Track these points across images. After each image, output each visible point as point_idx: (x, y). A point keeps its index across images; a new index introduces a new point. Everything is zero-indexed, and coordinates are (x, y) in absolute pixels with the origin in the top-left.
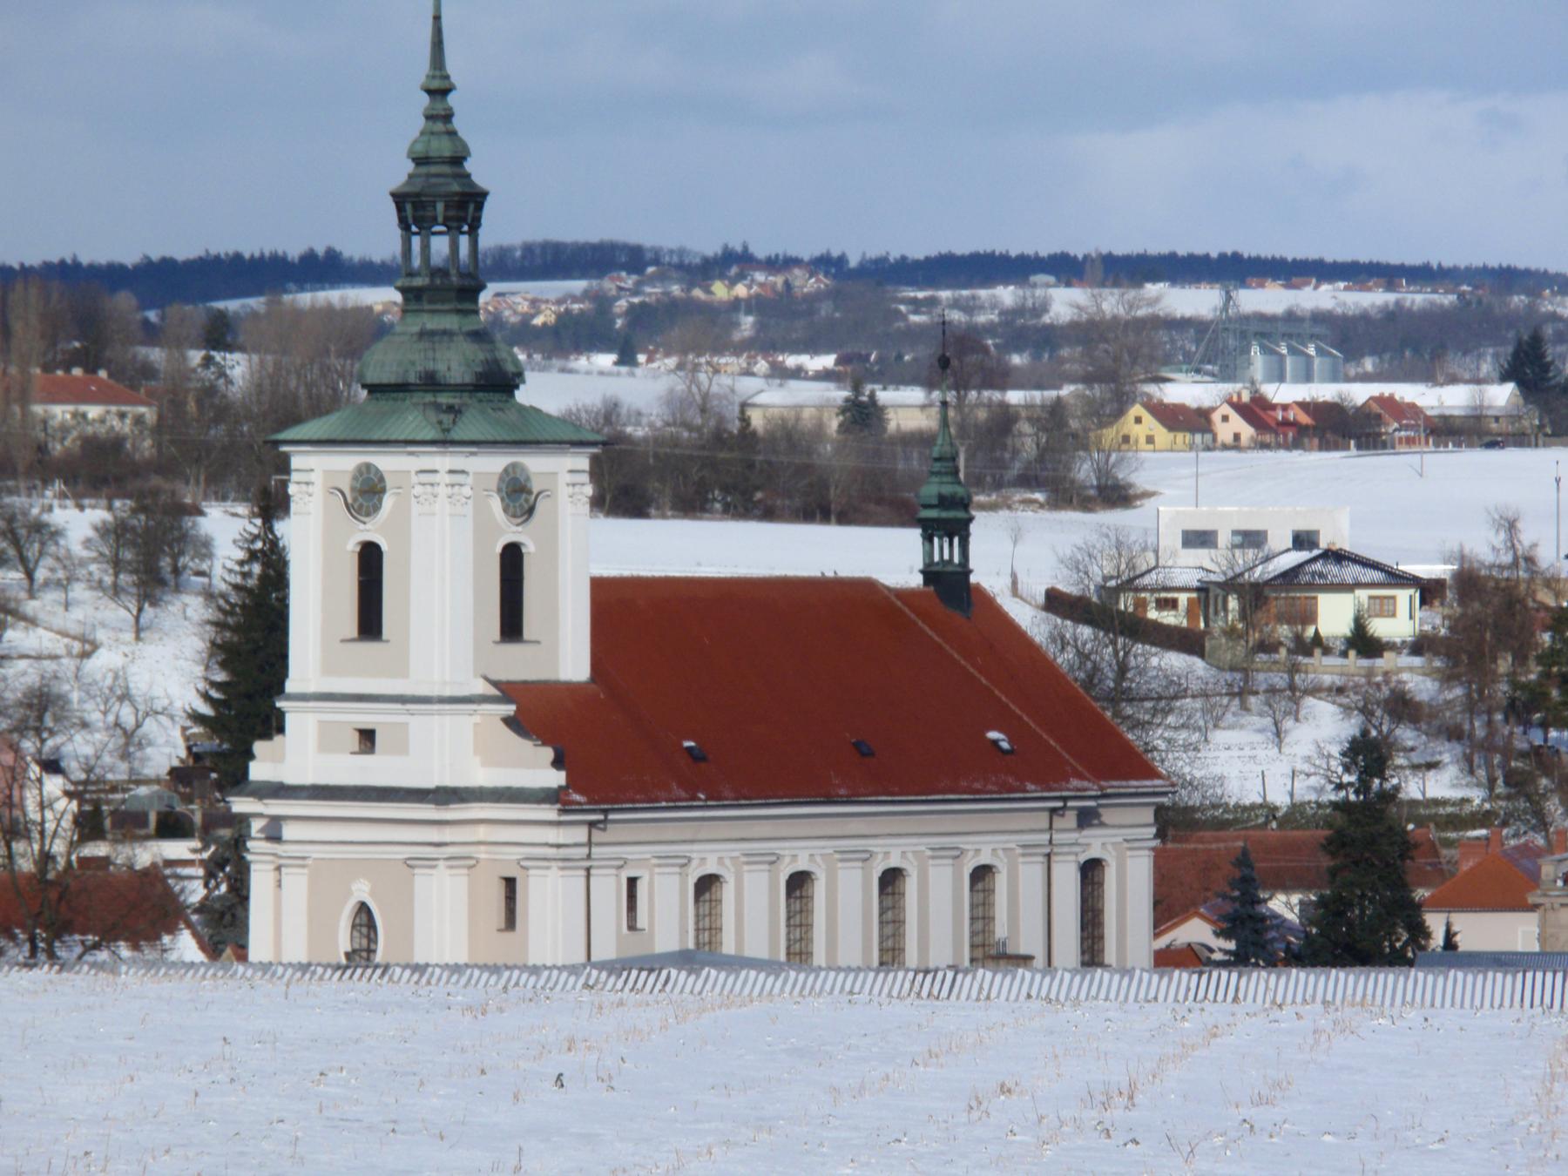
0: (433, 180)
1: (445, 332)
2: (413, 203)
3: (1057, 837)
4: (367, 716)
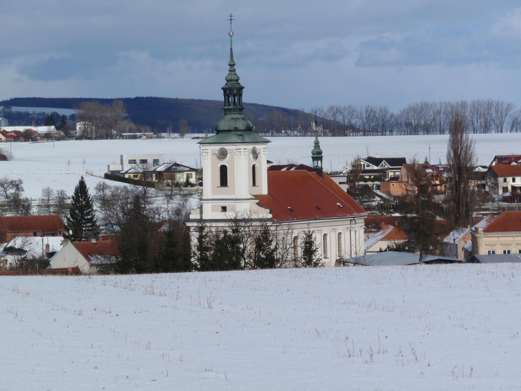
1: (237, 118)
3: (352, 226)
4: (224, 204)
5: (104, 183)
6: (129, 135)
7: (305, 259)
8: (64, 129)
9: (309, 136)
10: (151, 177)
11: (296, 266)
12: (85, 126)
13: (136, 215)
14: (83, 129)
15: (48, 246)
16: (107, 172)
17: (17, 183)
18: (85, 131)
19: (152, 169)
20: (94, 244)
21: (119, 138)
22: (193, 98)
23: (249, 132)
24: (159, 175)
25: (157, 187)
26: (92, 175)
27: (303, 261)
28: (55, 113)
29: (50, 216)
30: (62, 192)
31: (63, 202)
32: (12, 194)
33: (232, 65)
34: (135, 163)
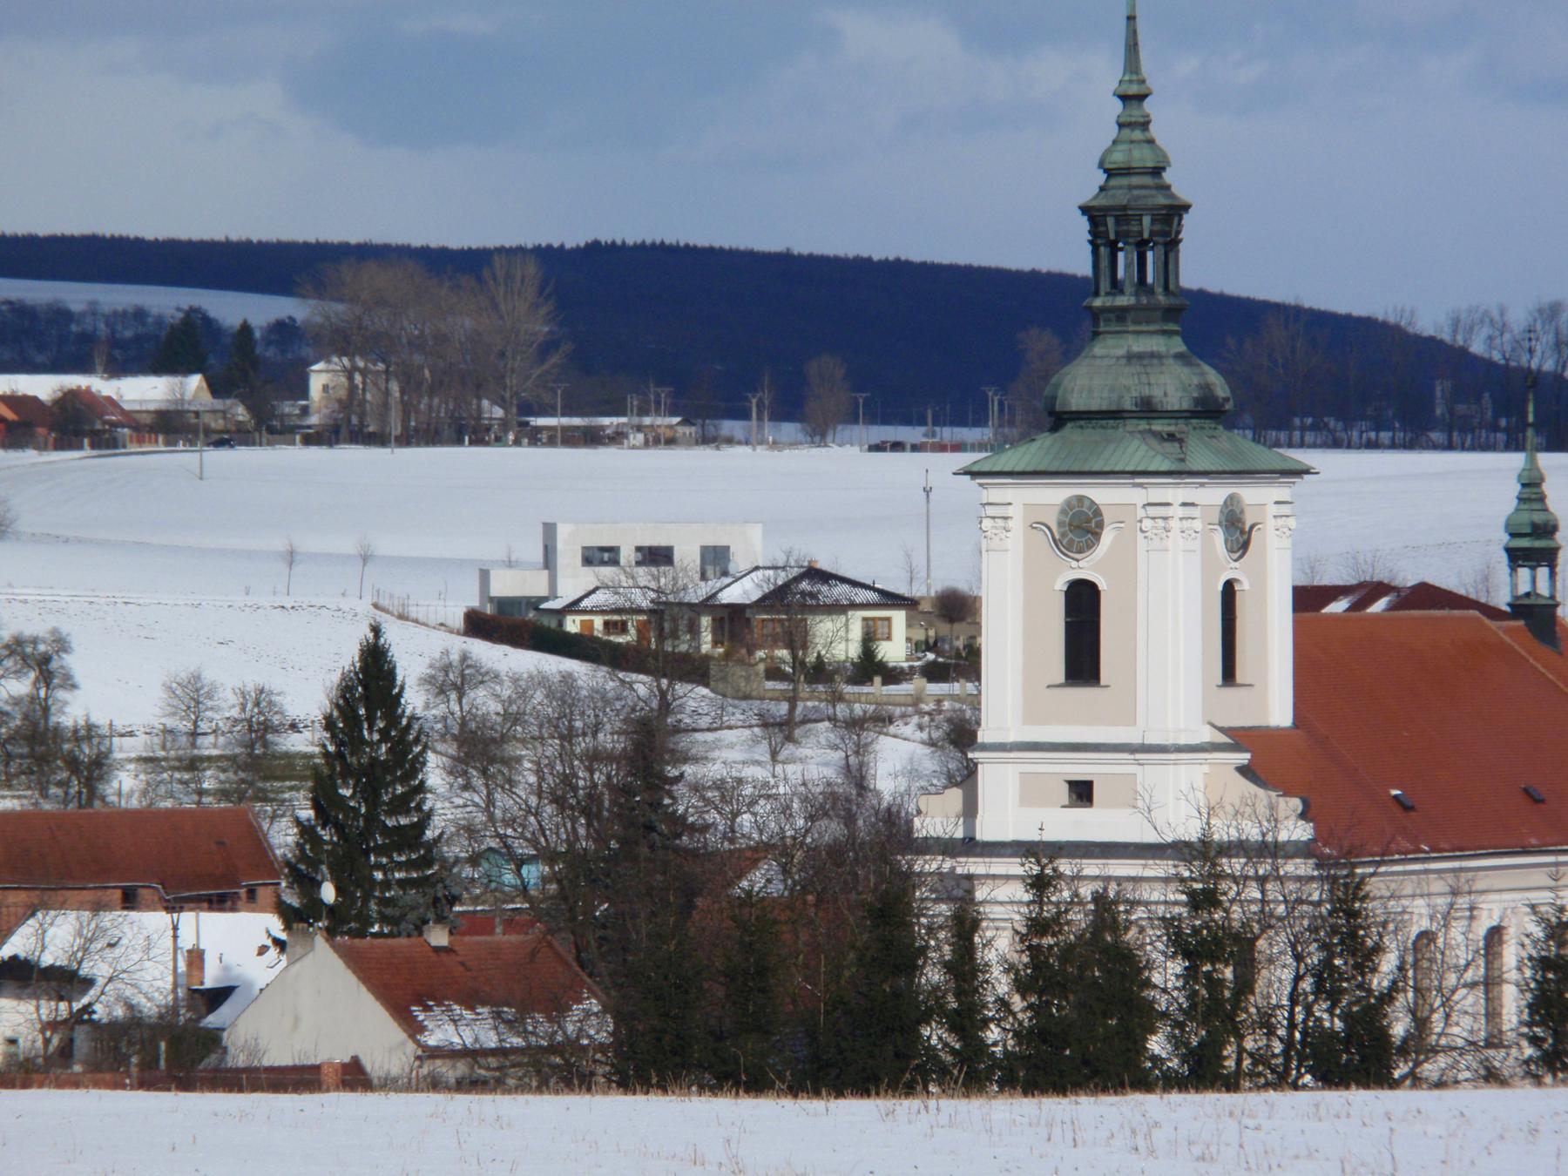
0: (1136, 192)
1: (1152, 355)
2: (1116, 217)
5: (464, 658)
6: (565, 429)
7: (1535, 1041)
8: (253, 390)
9: (1435, 447)
10: (675, 638)
11: (1492, 1077)
12: (350, 378)
13: (632, 818)
14: (342, 393)
15: (196, 958)
16: (475, 603)
17: (42, 648)
18: (350, 403)
19: (697, 592)
20: (438, 950)
21: (517, 443)
22: (865, 255)
23: (1208, 423)
24: (732, 620)
25: (724, 679)
26: (402, 617)
27: (1529, 1051)
28: (193, 311)
29: (200, 817)
30: (262, 698)
31: (266, 744)
32: (17, 701)
33: (1132, 98)
34: (615, 562)
